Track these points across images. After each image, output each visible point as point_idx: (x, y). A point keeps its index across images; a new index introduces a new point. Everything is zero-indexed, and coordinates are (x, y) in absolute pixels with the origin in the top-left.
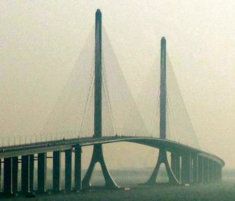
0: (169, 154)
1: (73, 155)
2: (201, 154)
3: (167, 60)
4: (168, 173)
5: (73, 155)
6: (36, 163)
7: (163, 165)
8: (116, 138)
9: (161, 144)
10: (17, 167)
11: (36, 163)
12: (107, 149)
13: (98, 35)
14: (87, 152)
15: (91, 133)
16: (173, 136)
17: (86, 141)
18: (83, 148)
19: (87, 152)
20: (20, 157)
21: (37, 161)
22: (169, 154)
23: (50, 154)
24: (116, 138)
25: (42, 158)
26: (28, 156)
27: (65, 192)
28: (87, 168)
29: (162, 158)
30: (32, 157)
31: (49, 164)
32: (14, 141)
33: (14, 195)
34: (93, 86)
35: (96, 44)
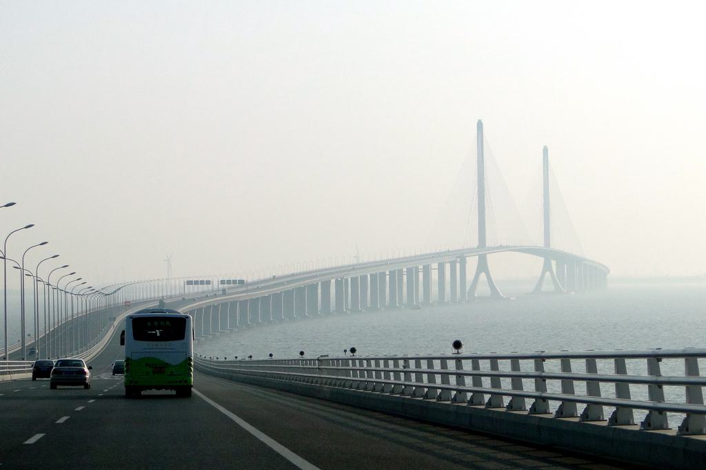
0: (554, 263)
1: (458, 265)
6: (421, 275)
7: (548, 274)
8: (501, 248)
9: (546, 253)
11: (421, 275)
12: (491, 259)
14: (472, 263)
16: (558, 244)
17: (471, 251)
19: (472, 263)
20: (405, 270)
22: (554, 263)
23: (435, 265)
24: (501, 248)
25: (427, 270)
26: (376, 274)
29: (547, 267)
30: (417, 268)
31: (435, 275)
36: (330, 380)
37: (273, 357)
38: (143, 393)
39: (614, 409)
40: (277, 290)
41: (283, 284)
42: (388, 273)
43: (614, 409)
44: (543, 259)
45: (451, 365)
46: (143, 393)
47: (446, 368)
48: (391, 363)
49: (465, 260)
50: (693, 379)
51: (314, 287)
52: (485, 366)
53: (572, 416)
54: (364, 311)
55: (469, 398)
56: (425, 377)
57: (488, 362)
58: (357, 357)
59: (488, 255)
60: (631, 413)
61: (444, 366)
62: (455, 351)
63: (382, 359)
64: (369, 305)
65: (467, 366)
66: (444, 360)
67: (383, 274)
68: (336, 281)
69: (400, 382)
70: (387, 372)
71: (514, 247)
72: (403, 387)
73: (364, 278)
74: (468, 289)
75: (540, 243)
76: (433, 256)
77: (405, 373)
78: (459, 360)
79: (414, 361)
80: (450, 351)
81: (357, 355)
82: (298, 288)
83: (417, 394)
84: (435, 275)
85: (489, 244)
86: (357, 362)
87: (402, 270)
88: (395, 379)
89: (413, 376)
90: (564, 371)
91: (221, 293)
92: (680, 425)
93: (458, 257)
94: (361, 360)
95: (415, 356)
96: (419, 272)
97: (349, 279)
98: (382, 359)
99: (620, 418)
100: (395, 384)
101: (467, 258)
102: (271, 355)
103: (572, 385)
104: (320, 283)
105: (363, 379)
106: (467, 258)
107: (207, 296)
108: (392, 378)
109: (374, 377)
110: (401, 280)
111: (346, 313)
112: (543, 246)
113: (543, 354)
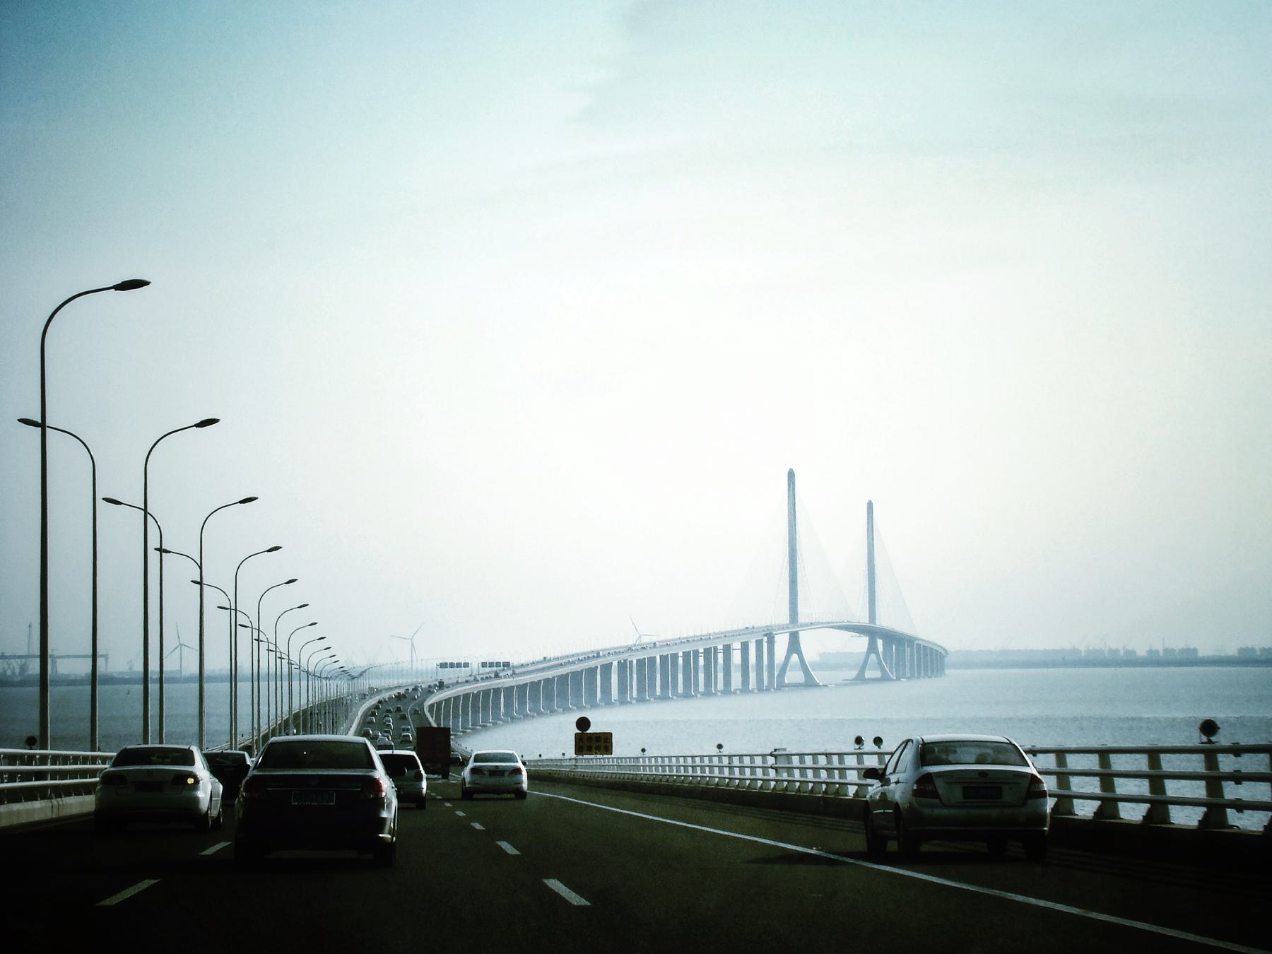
0: (880, 642)
1: (765, 645)
2: (920, 642)
3: (874, 526)
4: (801, 665)
5: (765, 645)
6: (720, 656)
7: (873, 656)
8: (812, 625)
9: (871, 632)
10: (677, 662)
11: (720, 656)
12: (804, 637)
13: (791, 500)
14: (782, 643)
15: (784, 618)
16: (886, 620)
17: (782, 628)
18: (777, 638)
19: (782, 643)
20: (720, 647)
21: (702, 658)
22: (880, 642)
23: (737, 645)
24: (812, 625)
25: (727, 649)
26: (668, 655)
27: (756, 691)
28: (783, 659)
29: (872, 648)
30: (716, 649)
31: (736, 657)
32: (453, 735)
33: (696, 696)
34: (787, 559)
35: (789, 512)
36: (631, 776)
37: (565, 756)
38: (925, 847)
39: (856, 787)
40: (549, 674)
41: (573, 663)
42: (681, 654)
43: (856, 787)
44: (868, 638)
45: (715, 760)
46: (925, 847)
47: (712, 762)
48: (666, 760)
49: (773, 637)
50: (802, 766)
51: (607, 668)
52: (809, 761)
53: (768, 789)
54: (675, 697)
55: (772, 787)
56: (716, 770)
57: (690, 758)
58: (647, 756)
59: (800, 632)
60: (1072, 805)
61: (710, 761)
62: (718, 750)
63: (706, 756)
64: (658, 694)
65: (725, 761)
66: (710, 757)
67: (675, 656)
68: (619, 662)
69: (833, 781)
70: (702, 767)
71: (829, 623)
72: (708, 779)
73: (652, 660)
74: (776, 673)
75: (862, 618)
76: (735, 634)
77: (693, 767)
78: (720, 757)
79: (653, 759)
80: (715, 751)
81: (647, 754)
82: (574, 672)
83: (829, 792)
84: (736, 657)
85: (802, 619)
86: (647, 759)
87: (697, 650)
88: (840, 778)
89: (707, 769)
90: (859, 764)
91: (493, 675)
92: (1200, 819)
93: (764, 635)
94: (650, 758)
95: (799, 752)
96: (698, 656)
97: (635, 662)
98: (706, 756)
99: (861, 794)
100: (677, 776)
101: (776, 636)
102: (540, 756)
103: (1068, 782)
104: (599, 667)
105: (645, 773)
106: (776, 636)
107: (457, 682)
108: (683, 771)
109: (675, 771)
110: (696, 662)
111: (715, 694)
112: (867, 622)
113: (1034, 749)
